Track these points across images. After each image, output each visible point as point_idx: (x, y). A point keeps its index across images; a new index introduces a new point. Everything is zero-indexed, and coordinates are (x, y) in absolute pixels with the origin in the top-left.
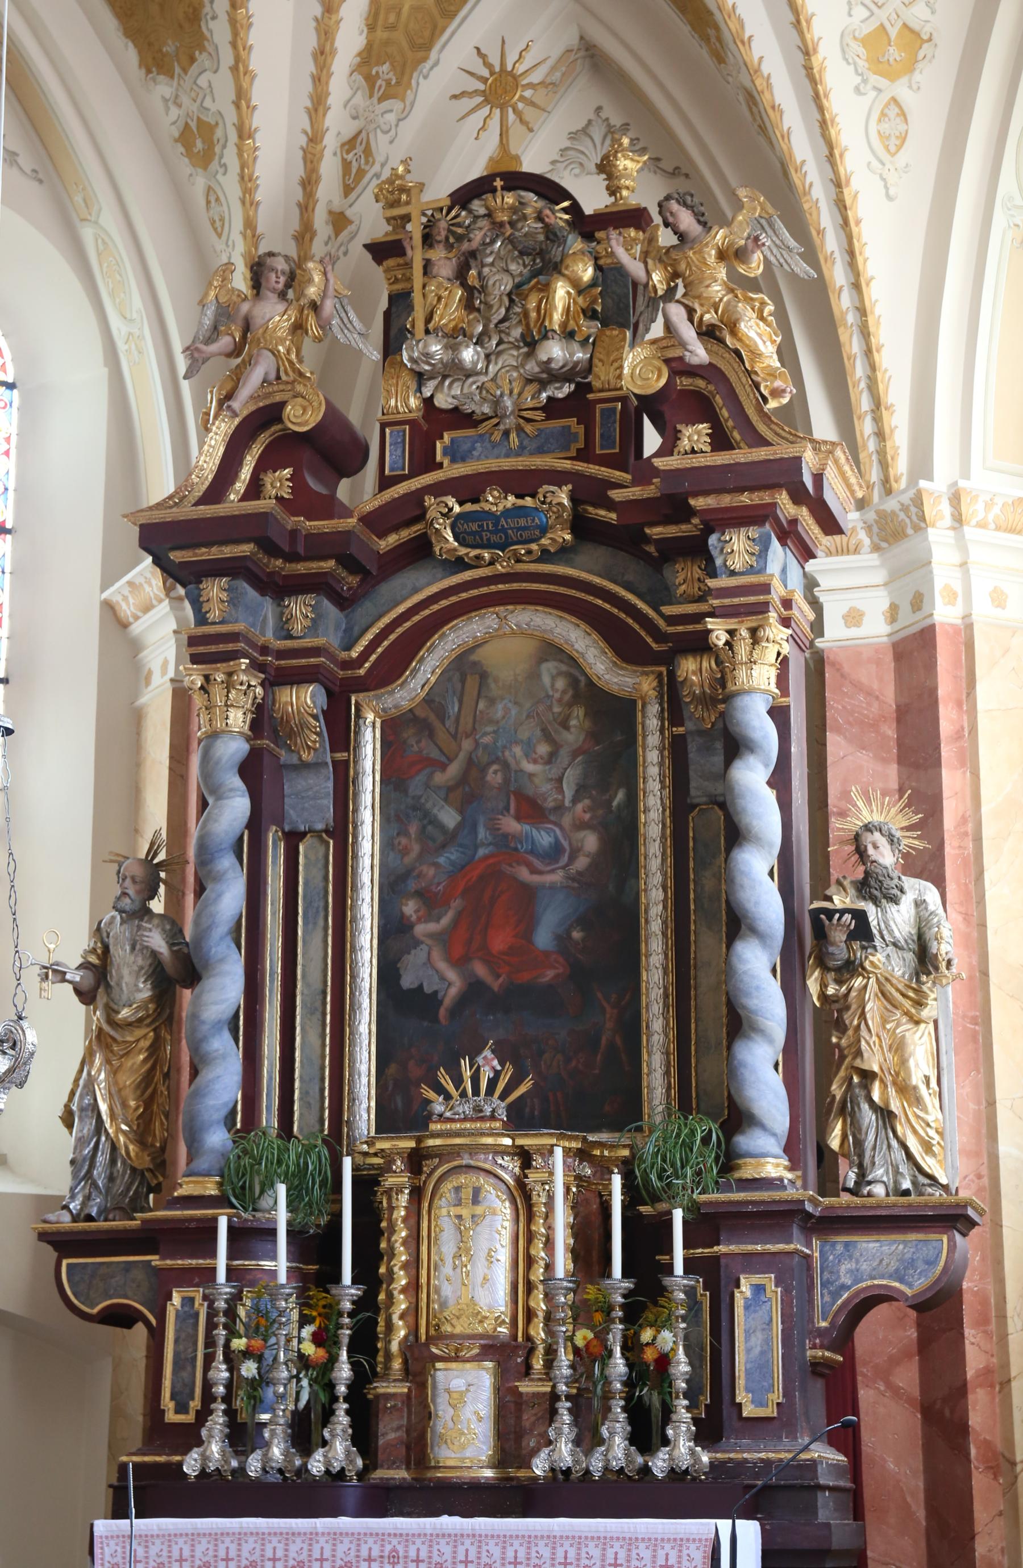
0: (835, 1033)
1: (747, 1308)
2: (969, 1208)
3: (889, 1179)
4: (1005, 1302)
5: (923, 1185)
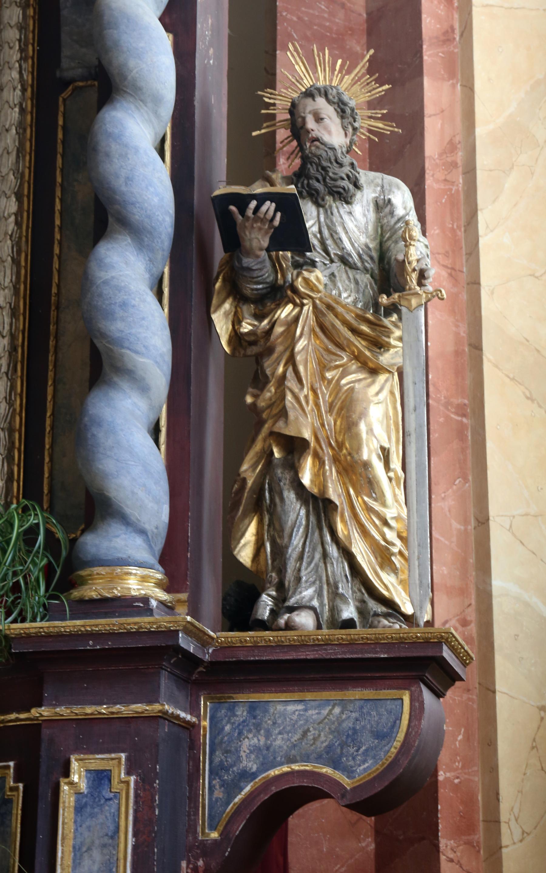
0: (250, 390)
1: (79, 809)
2: (445, 648)
3: (322, 604)
4: (498, 800)
5: (376, 615)
